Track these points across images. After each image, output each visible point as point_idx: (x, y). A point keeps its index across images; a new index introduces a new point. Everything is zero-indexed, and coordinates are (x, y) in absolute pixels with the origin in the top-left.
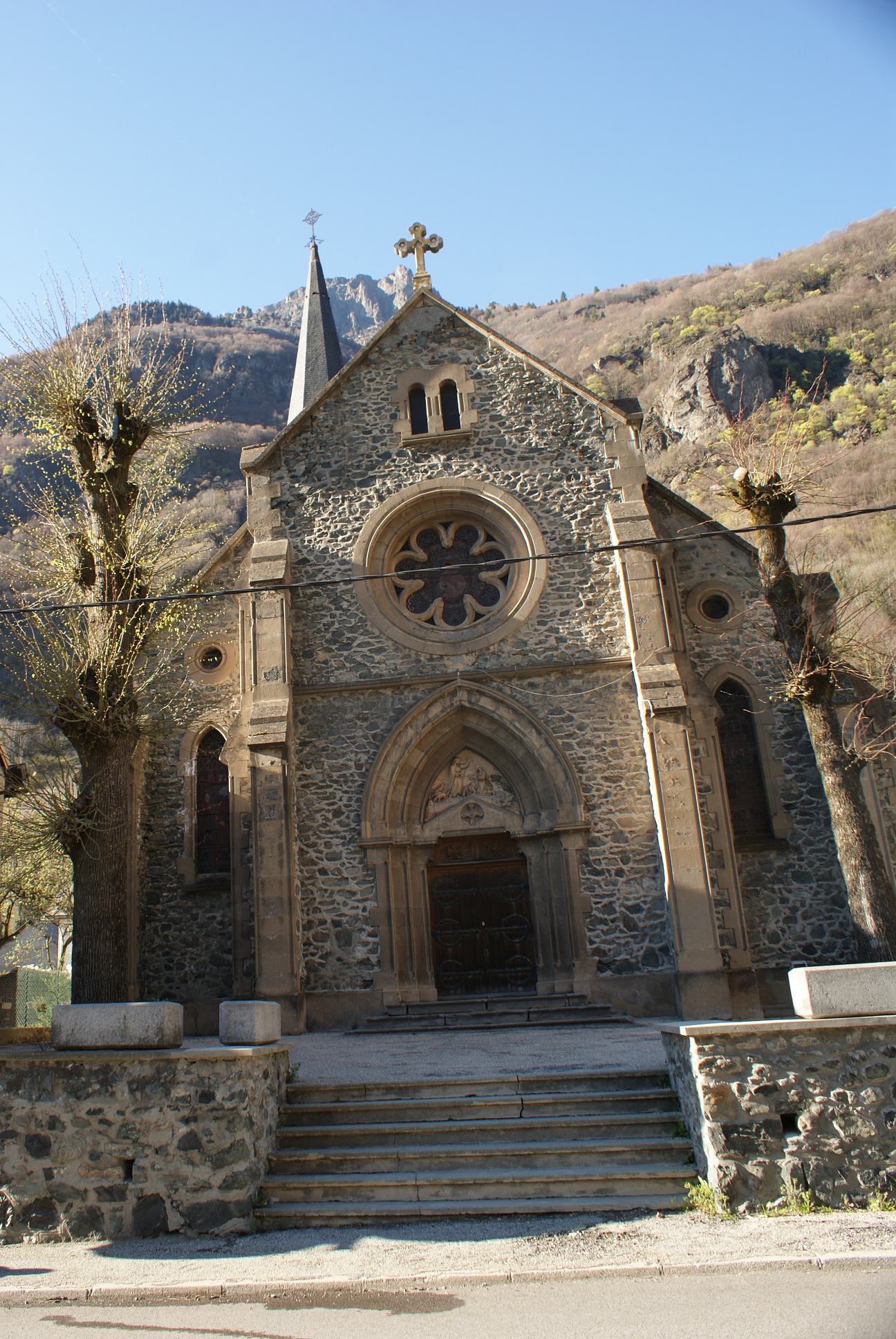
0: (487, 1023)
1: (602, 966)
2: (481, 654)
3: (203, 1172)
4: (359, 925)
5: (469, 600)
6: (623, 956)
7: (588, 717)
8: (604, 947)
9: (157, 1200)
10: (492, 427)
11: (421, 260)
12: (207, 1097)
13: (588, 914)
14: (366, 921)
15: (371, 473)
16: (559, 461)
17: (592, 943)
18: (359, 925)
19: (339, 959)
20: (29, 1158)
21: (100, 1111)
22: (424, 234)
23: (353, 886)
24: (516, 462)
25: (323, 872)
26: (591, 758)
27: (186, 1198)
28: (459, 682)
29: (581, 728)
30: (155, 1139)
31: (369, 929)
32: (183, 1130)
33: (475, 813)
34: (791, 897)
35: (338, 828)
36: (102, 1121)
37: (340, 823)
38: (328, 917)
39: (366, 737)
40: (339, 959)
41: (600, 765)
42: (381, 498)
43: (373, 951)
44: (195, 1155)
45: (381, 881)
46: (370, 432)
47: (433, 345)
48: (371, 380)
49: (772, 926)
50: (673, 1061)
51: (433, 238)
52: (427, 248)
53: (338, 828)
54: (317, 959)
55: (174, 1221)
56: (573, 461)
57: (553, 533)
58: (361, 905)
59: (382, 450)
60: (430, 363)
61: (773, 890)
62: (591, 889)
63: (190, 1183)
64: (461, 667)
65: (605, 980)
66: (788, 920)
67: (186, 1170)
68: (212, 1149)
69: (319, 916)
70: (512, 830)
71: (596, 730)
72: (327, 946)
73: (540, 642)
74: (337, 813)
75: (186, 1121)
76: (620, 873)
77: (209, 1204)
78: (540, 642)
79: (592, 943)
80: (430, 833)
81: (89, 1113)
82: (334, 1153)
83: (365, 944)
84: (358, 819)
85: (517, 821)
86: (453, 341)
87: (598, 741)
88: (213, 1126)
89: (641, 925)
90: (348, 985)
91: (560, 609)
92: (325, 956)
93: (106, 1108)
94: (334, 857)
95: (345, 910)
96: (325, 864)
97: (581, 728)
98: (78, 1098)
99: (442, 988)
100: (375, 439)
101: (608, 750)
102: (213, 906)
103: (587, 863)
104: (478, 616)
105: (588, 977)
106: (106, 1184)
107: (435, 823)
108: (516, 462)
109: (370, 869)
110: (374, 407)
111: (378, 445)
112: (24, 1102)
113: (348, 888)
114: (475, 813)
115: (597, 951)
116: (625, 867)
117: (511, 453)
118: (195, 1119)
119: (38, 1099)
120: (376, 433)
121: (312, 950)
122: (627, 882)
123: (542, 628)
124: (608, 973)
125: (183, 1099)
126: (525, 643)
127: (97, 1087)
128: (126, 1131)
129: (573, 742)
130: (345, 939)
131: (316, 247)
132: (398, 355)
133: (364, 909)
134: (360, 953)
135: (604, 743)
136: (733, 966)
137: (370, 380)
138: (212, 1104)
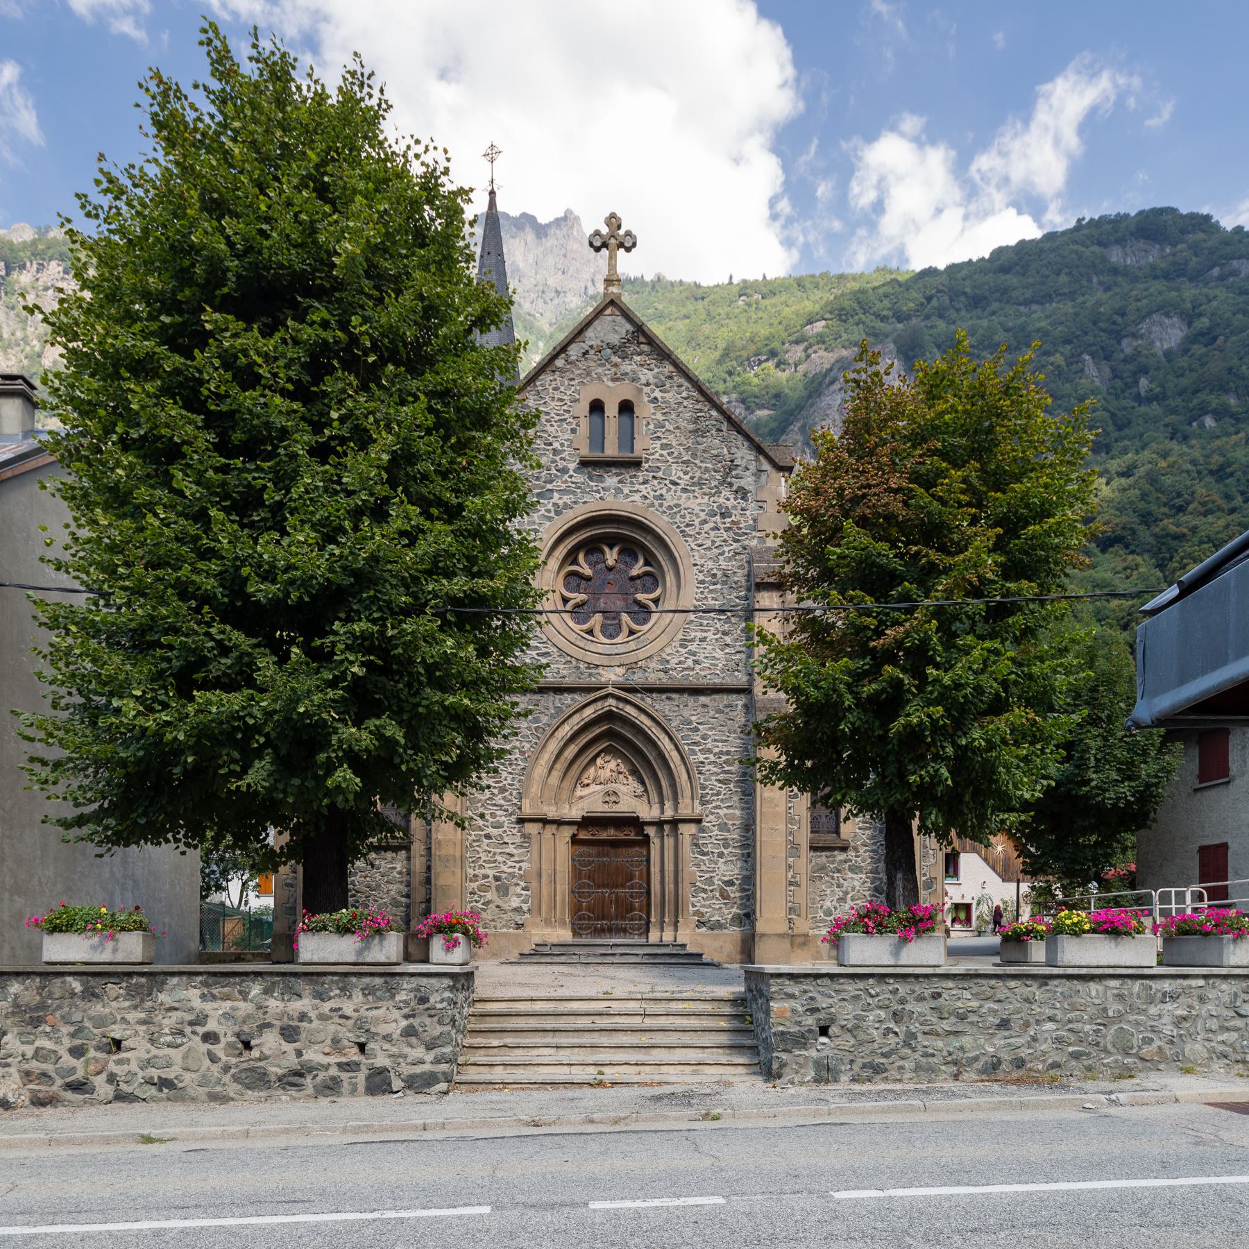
0: (606, 958)
1: (701, 924)
2: (631, 667)
3: (419, 1052)
4: (515, 880)
5: (625, 618)
6: (716, 918)
7: (711, 729)
8: (703, 910)
9: (383, 1071)
10: (661, 455)
11: (612, 258)
12: (423, 1000)
13: (693, 884)
14: (521, 877)
15: (549, 486)
16: (715, 498)
17: (694, 906)
18: (515, 880)
19: (498, 907)
20: (283, 1042)
21: (340, 1009)
22: (619, 227)
23: (510, 849)
24: (679, 493)
25: (488, 836)
26: (709, 764)
27: (407, 1070)
28: (611, 690)
29: (704, 737)
30: (383, 1029)
31: (523, 884)
32: (404, 1023)
33: (614, 798)
34: (846, 884)
35: (502, 802)
36: (341, 1017)
37: (504, 798)
38: (491, 873)
39: (529, 728)
40: (498, 907)
41: (715, 770)
42: (558, 513)
43: (525, 902)
44: (413, 1040)
45: (535, 847)
46: (551, 444)
47: (615, 359)
48: (555, 389)
49: (828, 904)
50: (751, 991)
51: (628, 234)
52: (621, 245)
53: (502, 802)
54: (479, 905)
55: (397, 1084)
56: (728, 499)
57: (702, 566)
58: (518, 865)
59: (561, 464)
60: (613, 380)
61: (833, 878)
62: (698, 865)
63: (409, 1060)
64: (613, 678)
65: (700, 934)
66: (840, 900)
67: (407, 1050)
68: (426, 1037)
69: (483, 871)
70: (641, 815)
71: (716, 741)
72: (489, 896)
73: (680, 662)
74: (502, 790)
75: (406, 1017)
76: (721, 855)
77: (424, 1073)
78: (680, 662)
79: (694, 906)
80: (576, 813)
81: (331, 1010)
82: (510, 1040)
83: (519, 895)
84: (520, 796)
85: (646, 807)
86: (637, 358)
87: (716, 750)
88: (428, 1021)
89: (732, 895)
90: (503, 927)
91: (700, 635)
92: (487, 903)
93: (344, 1007)
94: (497, 826)
95: (505, 868)
96: (490, 830)
97: (704, 737)
98: (322, 1000)
99: (575, 933)
100: (555, 452)
101: (724, 758)
102: (393, 859)
103: (697, 845)
104: (632, 632)
105: (688, 932)
106: (344, 1060)
107: (580, 805)
108: (679, 493)
109: (526, 837)
110: (557, 418)
111: (557, 458)
112: (279, 1003)
113: (507, 850)
114: (614, 798)
115: (697, 913)
116: (725, 852)
117: (675, 483)
118: (414, 1016)
119: (289, 1000)
120: (556, 445)
121: (476, 897)
122: (726, 863)
123: (684, 651)
124: (704, 929)
125: (405, 1002)
126: (668, 662)
127: (338, 992)
128: (360, 1025)
129: (697, 749)
130: (503, 891)
131: (492, 193)
132: (583, 364)
133: (520, 869)
134: (515, 902)
135: (721, 752)
136: (796, 931)
137: (554, 389)
138: (427, 1006)
